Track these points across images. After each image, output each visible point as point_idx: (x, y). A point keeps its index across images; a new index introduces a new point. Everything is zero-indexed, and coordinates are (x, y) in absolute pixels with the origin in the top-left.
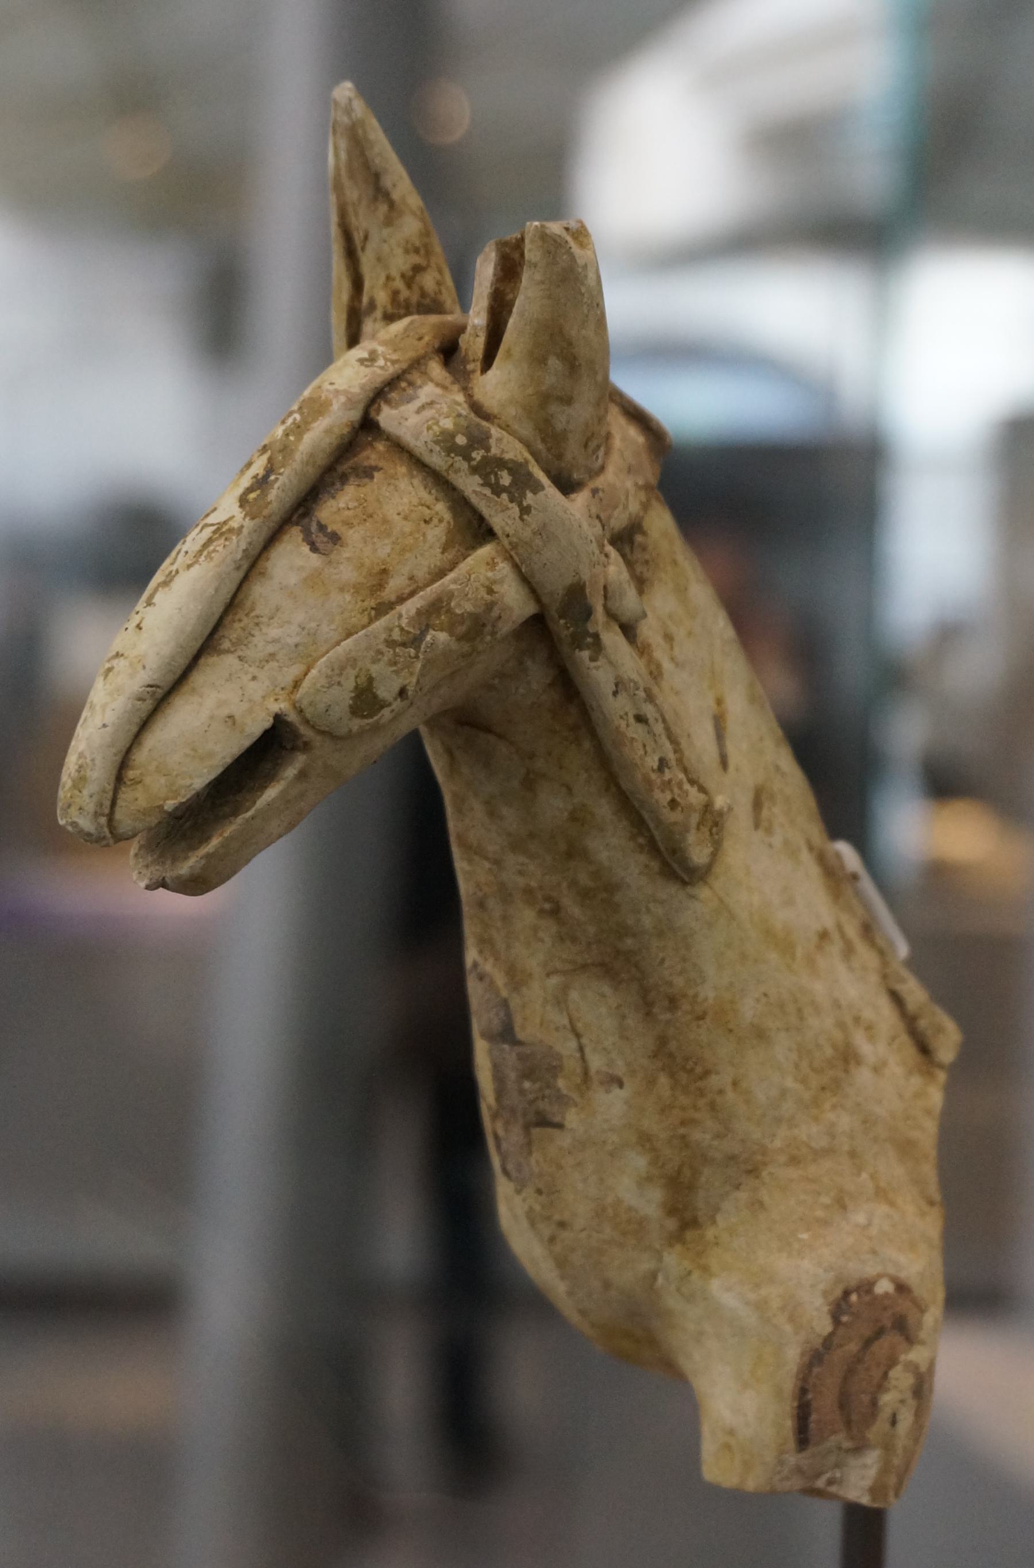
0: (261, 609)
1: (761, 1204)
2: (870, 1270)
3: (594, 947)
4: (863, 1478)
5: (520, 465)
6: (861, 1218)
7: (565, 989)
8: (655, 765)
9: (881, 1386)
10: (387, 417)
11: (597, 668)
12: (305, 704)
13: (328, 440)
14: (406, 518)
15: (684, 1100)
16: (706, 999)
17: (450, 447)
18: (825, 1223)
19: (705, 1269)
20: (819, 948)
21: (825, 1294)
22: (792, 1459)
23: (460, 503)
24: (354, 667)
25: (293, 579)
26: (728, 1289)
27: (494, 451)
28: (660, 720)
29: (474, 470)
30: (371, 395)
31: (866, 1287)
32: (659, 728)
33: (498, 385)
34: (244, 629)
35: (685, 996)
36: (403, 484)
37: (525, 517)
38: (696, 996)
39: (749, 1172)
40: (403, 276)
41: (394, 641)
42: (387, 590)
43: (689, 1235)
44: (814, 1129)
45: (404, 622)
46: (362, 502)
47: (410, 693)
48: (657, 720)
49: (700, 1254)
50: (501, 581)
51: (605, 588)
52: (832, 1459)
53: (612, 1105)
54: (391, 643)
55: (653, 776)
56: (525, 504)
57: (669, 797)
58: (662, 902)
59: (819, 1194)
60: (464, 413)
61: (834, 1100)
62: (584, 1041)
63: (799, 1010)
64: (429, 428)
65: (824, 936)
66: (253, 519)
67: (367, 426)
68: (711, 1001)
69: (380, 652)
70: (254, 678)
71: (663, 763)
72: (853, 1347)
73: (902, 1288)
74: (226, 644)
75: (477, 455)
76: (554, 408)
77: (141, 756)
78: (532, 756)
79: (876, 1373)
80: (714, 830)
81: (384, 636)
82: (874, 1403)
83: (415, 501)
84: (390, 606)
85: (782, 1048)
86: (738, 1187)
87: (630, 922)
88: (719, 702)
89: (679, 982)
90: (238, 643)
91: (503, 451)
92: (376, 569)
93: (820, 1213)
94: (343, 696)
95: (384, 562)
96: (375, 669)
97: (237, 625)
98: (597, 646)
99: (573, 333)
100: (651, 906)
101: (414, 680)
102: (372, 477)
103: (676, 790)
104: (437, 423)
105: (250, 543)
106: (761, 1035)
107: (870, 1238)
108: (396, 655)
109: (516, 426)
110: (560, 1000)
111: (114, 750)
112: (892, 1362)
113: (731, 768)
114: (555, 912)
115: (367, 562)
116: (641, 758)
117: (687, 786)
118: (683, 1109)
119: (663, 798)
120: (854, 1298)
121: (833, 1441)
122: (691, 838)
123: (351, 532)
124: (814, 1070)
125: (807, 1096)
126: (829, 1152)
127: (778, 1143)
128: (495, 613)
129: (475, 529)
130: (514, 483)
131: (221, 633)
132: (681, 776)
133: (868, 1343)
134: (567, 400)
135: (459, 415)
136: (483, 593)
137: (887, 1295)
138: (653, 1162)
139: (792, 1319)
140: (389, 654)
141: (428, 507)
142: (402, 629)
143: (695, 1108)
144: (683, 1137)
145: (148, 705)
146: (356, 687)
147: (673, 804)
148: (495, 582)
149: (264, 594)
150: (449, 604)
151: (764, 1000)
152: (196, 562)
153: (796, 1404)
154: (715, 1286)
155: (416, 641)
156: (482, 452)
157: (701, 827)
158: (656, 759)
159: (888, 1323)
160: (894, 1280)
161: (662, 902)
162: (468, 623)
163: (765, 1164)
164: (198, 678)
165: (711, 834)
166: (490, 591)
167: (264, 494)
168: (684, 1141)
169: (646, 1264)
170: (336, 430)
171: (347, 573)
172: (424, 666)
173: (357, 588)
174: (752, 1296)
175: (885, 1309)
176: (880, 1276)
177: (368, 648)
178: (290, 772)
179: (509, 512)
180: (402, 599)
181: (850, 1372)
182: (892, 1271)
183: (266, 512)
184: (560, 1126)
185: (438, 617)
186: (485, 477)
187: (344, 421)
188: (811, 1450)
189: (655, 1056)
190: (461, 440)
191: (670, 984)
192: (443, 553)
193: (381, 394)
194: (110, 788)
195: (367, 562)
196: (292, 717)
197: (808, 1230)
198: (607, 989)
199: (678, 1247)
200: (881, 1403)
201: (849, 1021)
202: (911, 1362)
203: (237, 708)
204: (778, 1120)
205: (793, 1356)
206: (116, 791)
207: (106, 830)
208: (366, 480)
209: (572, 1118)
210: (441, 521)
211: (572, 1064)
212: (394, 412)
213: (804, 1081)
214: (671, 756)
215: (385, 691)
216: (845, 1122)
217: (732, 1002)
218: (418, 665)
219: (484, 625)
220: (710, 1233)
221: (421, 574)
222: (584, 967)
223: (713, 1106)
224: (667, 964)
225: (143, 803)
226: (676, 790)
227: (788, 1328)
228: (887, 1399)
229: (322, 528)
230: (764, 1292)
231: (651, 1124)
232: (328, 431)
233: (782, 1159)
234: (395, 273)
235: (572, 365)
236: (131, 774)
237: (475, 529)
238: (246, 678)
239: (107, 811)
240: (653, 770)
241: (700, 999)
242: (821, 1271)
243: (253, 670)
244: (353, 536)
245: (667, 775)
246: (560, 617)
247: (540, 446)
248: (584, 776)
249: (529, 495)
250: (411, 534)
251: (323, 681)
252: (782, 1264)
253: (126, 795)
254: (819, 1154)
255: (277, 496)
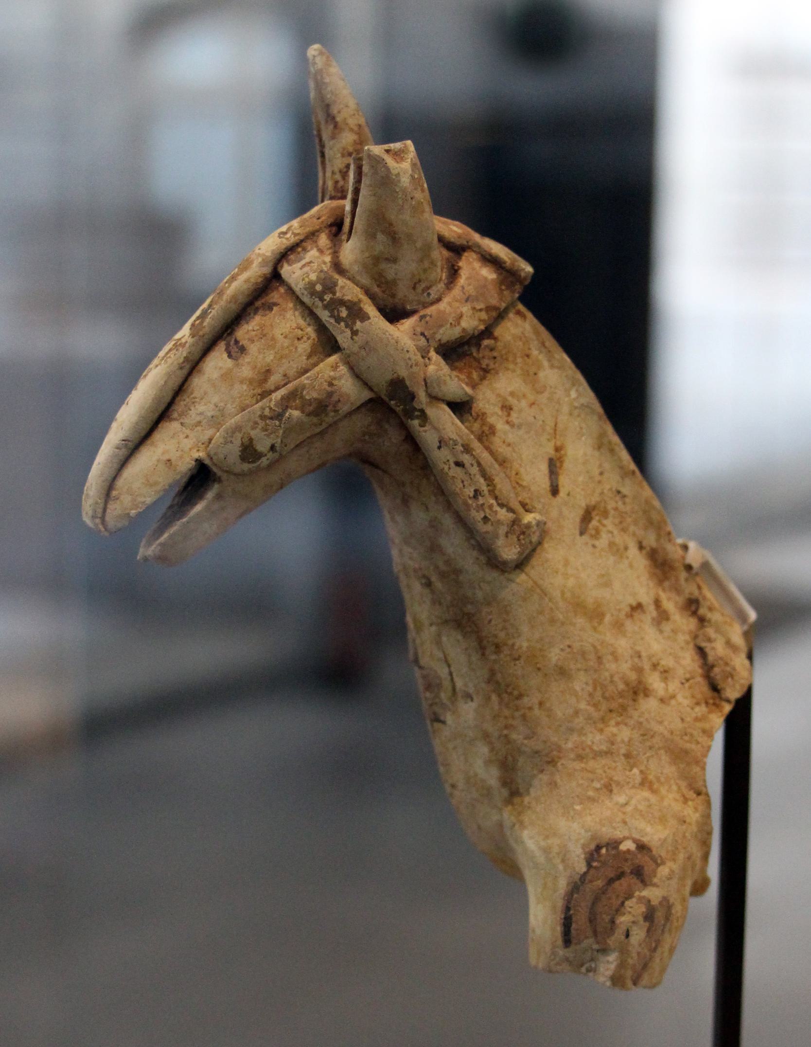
0: (197, 394)
1: (556, 784)
2: (618, 834)
3: (451, 609)
4: (608, 969)
5: (355, 304)
6: (622, 799)
7: (439, 635)
8: (472, 494)
9: (619, 910)
10: (286, 270)
11: (425, 431)
12: (212, 453)
13: (245, 287)
14: (286, 337)
15: (507, 712)
16: (521, 647)
17: (313, 293)
18: (592, 800)
19: (521, 823)
20: (630, 616)
21: (584, 846)
22: (561, 952)
23: (321, 328)
24: (240, 431)
25: (215, 375)
26: (531, 838)
27: (338, 295)
28: (475, 465)
29: (326, 307)
30: (278, 257)
31: (614, 844)
32: (475, 470)
33: (351, 251)
34: (185, 406)
35: (505, 644)
36: (289, 314)
37: (355, 337)
38: (513, 645)
39: (549, 763)
40: (340, 172)
41: (265, 416)
42: (269, 383)
43: (516, 800)
44: (598, 737)
45: (273, 403)
46: (262, 327)
47: (278, 449)
48: (472, 465)
49: (520, 813)
50: (340, 378)
51: (425, 380)
52: (589, 954)
53: (468, 711)
54: (263, 417)
55: (470, 502)
56: (355, 329)
57: (482, 516)
58: (489, 583)
59: (592, 781)
60: (325, 269)
61: (619, 719)
62: (452, 669)
63: (599, 658)
64: (303, 280)
65: (638, 607)
66: (193, 337)
67: (274, 277)
68: (524, 649)
69: (256, 423)
70: (187, 437)
71: (477, 493)
72: (600, 883)
73: (642, 847)
74: (175, 415)
75: (328, 297)
76: (383, 266)
77: (120, 483)
78: (403, 484)
79: (616, 903)
80: (522, 537)
81: (259, 413)
82: (613, 922)
83: (294, 325)
84: (271, 392)
85: (580, 683)
86: (542, 771)
87: (469, 594)
88: (557, 449)
89: (502, 635)
90: (182, 414)
91: (344, 295)
92: (264, 370)
93: (591, 793)
94: (235, 449)
95: (268, 365)
96: (253, 433)
97: (182, 403)
98: (423, 417)
99: (393, 217)
100: (482, 584)
101: (279, 440)
102: (272, 309)
103: (487, 510)
104: (308, 277)
105: (190, 353)
106: (562, 672)
107: (624, 813)
108: (267, 425)
109: (358, 278)
110: (438, 643)
111: (103, 478)
112: (629, 896)
113: (562, 493)
114: (429, 584)
115: (259, 365)
116: (460, 489)
117: (498, 509)
118: (506, 717)
119: (479, 516)
120: (604, 851)
121: (586, 943)
122: (500, 542)
123: (252, 346)
124: (604, 698)
125: (596, 715)
126: (608, 753)
127: (570, 745)
128: (335, 398)
129: (328, 344)
130: (349, 315)
131: (173, 408)
132: (493, 501)
133: (611, 881)
134: (394, 260)
135: (321, 271)
136: (325, 386)
137: (628, 851)
138: (492, 750)
139: (563, 861)
140: (262, 424)
141: (302, 330)
142: (271, 409)
143: (513, 718)
144: (506, 736)
145: (124, 452)
146: (242, 444)
147: (486, 519)
148: (335, 379)
149: (199, 383)
150: (302, 393)
151: (568, 650)
152: (160, 364)
153: (563, 917)
154: (525, 834)
155: (279, 416)
156: (330, 296)
157: (509, 535)
158: (472, 490)
159: (628, 870)
160: (635, 841)
161: (489, 583)
162: (314, 405)
163: (560, 758)
164: (157, 436)
165: (519, 540)
166: (331, 384)
167: (202, 322)
168: (508, 740)
169: (495, 817)
170: (253, 280)
171: (246, 372)
172: (284, 432)
173: (251, 381)
174: (543, 843)
175: (626, 860)
176: (625, 838)
177: (249, 420)
178: (210, 495)
179: (345, 334)
180: (277, 388)
181: (596, 900)
182: (636, 836)
183: (201, 333)
184: (444, 722)
185: (294, 401)
186: (332, 311)
187: (259, 273)
188: (573, 947)
189: (489, 682)
190: (319, 288)
191: (496, 636)
192: (307, 359)
193: (285, 255)
194: (101, 502)
195: (259, 365)
196: (207, 462)
197: (581, 803)
198: (460, 637)
199: (510, 807)
200: (618, 922)
201: (647, 666)
202: (644, 897)
203: (173, 455)
204: (571, 730)
205: (563, 885)
206: (106, 503)
207: (101, 526)
208: (268, 312)
209: (449, 718)
210: (308, 339)
211: (447, 683)
212: (290, 268)
213: (595, 705)
214: (484, 488)
215: (262, 446)
216: (625, 734)
217: (541, 650)
218: (281, 431)
219: (327, 406)
220: (527, 800)
221: (292, 373)
222: (446, 622)
223: (524, 717)
224: (493, 622)
225: (119, 512)
226: (487, 510)
227: (561, 867)
228: (623, 920)
229: (237, 342)
230: (550, 841)
231: (489, 727)
232: (247, 281)
233: (572, 756)
234: (336, 170)
235: (394, 238)
236: (114, 493)
237: (328, 344)
238: (182, 436)
239: (99, 515)
240: (470, 498)
241: (516, 647)
242: (583, 831)
243: (188, 432)
244: (253, 349)
245: (481, 501)
246: (391, 400)
247: (376, 289)
248: (433, 498)
249: (358, 323)
250: (288, 347)
251: (222, 440)
252: (562, 824)
253: (111, 506)
254: (598, 755)
255: (209, 323)
